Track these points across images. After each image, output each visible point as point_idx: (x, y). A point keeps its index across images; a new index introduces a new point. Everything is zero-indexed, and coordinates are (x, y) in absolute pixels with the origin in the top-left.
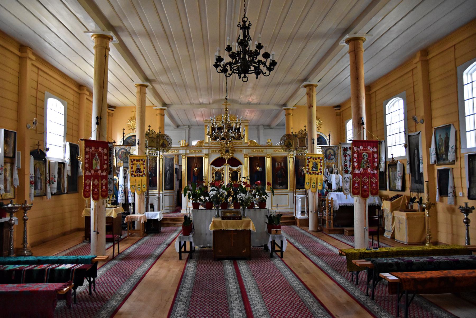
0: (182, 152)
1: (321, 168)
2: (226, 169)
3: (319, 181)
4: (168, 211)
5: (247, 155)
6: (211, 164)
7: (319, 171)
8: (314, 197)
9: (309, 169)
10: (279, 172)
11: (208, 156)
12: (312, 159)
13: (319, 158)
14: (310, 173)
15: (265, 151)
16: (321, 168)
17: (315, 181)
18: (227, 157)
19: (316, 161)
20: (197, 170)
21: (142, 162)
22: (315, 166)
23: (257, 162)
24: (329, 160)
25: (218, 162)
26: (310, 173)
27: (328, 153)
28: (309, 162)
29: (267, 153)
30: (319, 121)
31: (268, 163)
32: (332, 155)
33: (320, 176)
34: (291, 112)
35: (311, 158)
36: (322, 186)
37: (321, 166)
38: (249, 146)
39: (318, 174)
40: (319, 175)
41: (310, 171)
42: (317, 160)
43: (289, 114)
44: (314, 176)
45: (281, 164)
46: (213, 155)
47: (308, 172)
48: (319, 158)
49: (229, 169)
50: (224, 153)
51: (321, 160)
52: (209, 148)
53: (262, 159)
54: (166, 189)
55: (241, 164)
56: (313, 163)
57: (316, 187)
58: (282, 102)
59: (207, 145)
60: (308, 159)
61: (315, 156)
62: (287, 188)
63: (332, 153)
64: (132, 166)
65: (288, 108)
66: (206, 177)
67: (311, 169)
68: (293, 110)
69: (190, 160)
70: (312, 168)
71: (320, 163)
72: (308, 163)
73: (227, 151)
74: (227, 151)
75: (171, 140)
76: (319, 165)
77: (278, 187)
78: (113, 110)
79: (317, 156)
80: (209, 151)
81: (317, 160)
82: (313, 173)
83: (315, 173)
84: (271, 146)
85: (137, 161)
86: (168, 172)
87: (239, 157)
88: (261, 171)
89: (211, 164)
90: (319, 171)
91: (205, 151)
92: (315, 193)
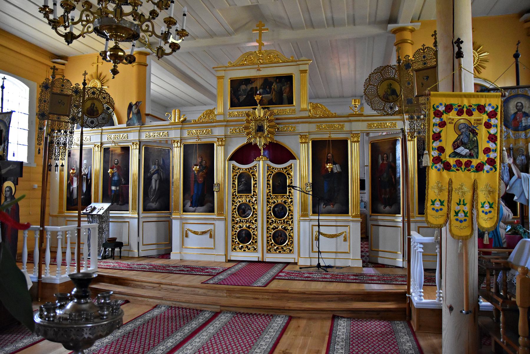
0: (174, 134)
2: (261, 167)
3: (482, 197)
4: (154, 253)
5: (305, 137)
6: (231, 159)
7: (482, 158)
8: (462, 256)
9: (441, 150)
10: (385, 175)
11: (224, 141)
12: (453, 115)
14: (447, 167)
15: (347, 127)
16: (491, 145)
17: (468, 197)
18: (260, 142)
19: (472, 119)
20: (199, 171)
22: (467, 138)
23: (329, 153)
24: (516, 129)
25: (244, 155)
26: (447, 167)
28: (443, 124)
29: (351, 132)
30: (480, 53)
33: (483, 178)
34: (407, 35)
35: (449, 108)
36: (494, 214)
37: (492, 138)
38: (309, 117)
39: (479, 168)
40: (483, 175)
41: (446, 157)
42: (476, 115)
43: (404, 41)
44: (462, 178)
45: (387, 157)
46: (235, 139)
47: (437, 160)
49: (269, 167)
50: (253, 133)
51: (492, 115)
52: (226, 123)
53: (341, 147)
54: (146, 209)
55: (294, 158)
56: (457, 127)
57: (471, 217)
58: (383, 13)
59: (221, 118)
60: (438, 114)
61: (466, 102)
62: (345, 211)
64: (437, 129)
65: (400, 25)
66: (218, 185)
67: (449, 150)
68: (412, 31)
69: (187, 149)
70: (456, 145)
72: (437, 129)
73: (260, 129)
74: (260, 129)
76: (483, 133)
77: (381, 207)
78: (64, 64)
80: (226, 131)
81: (476, 115)
84: (361, 115)
85: (460, 113)
86: (155, 176)
87: (288, 142)
88: (339, 173)
89: (231, 159)
90: (482, 158)
91: (219, 132)
92: (465, 240)
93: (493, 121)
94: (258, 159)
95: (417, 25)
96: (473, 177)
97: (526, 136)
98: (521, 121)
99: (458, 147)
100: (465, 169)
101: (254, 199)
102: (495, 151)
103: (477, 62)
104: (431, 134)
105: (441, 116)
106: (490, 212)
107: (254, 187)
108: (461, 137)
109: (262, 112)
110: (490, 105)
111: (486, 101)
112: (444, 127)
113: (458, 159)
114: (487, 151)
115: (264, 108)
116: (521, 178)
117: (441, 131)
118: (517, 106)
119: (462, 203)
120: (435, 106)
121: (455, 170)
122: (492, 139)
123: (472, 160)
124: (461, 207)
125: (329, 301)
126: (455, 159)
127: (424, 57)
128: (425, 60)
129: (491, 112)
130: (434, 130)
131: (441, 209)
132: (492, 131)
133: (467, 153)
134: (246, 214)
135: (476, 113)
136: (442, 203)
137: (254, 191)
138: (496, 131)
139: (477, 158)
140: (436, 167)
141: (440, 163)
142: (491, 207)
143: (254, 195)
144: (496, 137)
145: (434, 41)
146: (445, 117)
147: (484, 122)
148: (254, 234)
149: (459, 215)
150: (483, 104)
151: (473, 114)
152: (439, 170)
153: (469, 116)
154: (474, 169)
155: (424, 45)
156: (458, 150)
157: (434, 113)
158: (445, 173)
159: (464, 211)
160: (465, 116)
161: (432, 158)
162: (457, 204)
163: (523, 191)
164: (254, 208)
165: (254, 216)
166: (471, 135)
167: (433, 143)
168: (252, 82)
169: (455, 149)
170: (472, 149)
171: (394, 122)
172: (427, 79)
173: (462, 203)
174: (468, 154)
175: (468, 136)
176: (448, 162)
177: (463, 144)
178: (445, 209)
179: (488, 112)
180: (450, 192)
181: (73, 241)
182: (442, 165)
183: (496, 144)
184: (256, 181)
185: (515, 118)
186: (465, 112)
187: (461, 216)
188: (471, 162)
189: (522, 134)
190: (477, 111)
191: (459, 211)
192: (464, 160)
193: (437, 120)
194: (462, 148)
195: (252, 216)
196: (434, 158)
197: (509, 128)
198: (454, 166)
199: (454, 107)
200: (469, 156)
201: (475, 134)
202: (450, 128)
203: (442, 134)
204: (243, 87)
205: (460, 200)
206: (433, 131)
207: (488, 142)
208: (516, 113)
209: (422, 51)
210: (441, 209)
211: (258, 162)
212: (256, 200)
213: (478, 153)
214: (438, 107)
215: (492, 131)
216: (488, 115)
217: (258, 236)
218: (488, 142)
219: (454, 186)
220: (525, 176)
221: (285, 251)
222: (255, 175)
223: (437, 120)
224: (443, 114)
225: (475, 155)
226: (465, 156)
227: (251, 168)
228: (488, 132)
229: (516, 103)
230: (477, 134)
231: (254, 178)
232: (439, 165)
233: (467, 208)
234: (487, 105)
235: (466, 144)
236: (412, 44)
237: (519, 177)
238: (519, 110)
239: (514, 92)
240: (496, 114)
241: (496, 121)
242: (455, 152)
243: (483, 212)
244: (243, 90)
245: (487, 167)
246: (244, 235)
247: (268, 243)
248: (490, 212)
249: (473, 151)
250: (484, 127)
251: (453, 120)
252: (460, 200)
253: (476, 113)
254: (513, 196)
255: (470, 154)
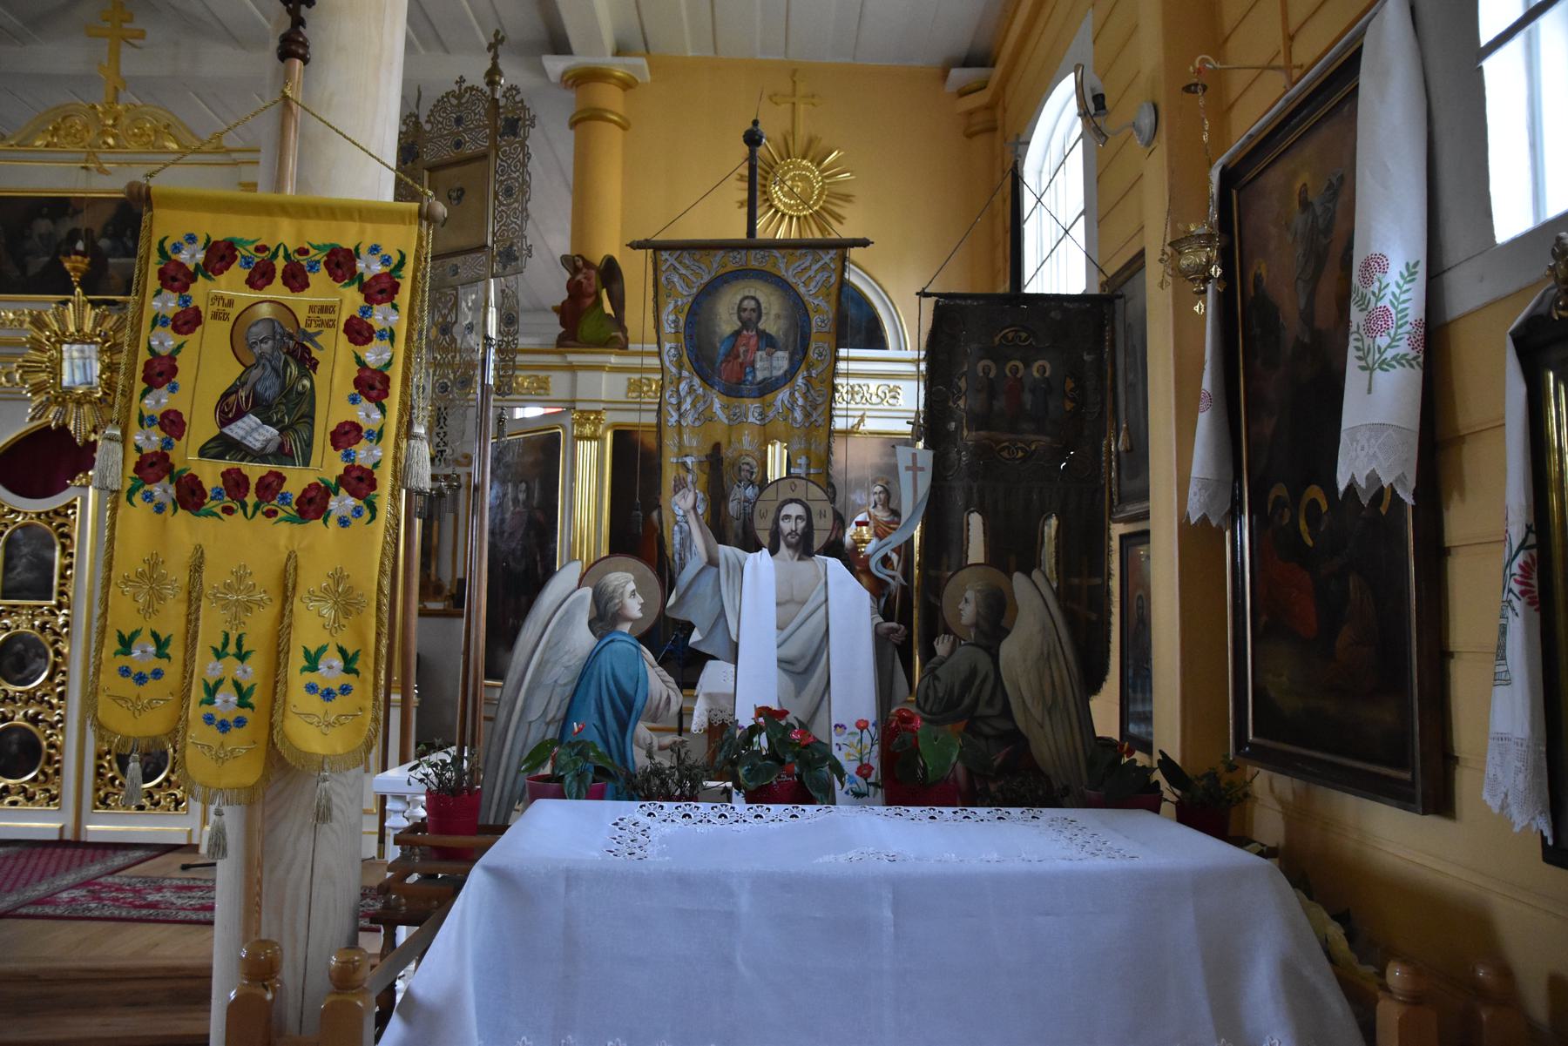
1: (364, 414)
3: (312, 624)
7: (328, 464)
9: (173, 424)
12: (232, 285)
13: (341, 263)
14: (190, 496)
16: (364, 414)
17: (258, 628)
19: (301, 302)
21: (350, 300)
22: (277, 383)
24: (733, 391)
27: (726, 320)
28: (188, 321)
31: (332, 316)
32: (769, 342)
34: (610, 98)
35: (221, 255)
37: (371, 385)
39: (312, 505)
41: (186, 455)
48: (341, 263)
51: (381, 290)
56: (239, 341)
61: (286, 234)
63: (771, 324)
64: (167, 341)
67: (203, 427)
68: (627, 85)
70: (228, 411)
71: (358, 332)
72: (167, 341)
75: (1016, 610)
76: (337, 365)
79: (320, 234)
81: (321, 289)
82: (235, 484)
83: (270, 487)
85: (260, 276)
93: (380, 317)
94: (80, 479)
95: (636, 65)
96: (283, 542)
97: (763, 415)
98: (752, 364)
99: (240, 414)
100: (257, 507)
101: (61, 620)
102: (379, 436)
103: (820, 195)
104: (143, 356)
105: (186, 288)
106: (345, 690)
107: (63, 576)
108: (256, 373)
109: (90, 315)
110: (374, 249)
111: (362, 232)
112: (191, 331)
113: (235, 464)
114: (346, 435)
115: (95, 304)
116: (717, 566)
117: (179, 348)
118: (741, 309)
119: (232, 648)
120: (168, 245)
121: (218, 510)
122: (372, 387)
123: (287, 470)
124: (231, 669)
125: (133, 1005)
126: (224, 465)
127: (459, 121)
128: (458, 133)
129: (377, 277)
130: (155, 343)
131: (157, 674)
132: (373, 355)
133: (268, 441)
134: (27, 672)
135: (319, 279)
136: (161, 645)
137: (62, 593)
138: (386, 356)
139: (306, 463)
140: (148, 497)
141: (166, 480)
142: (349, 669)
143: (60, 606)
144: (386, 381)
145: (489, 65)
146: (200, 291)
147: (344, 317)
148: (51, 746)
149: (219, 700)
150: (349, 244)
151: (308, 285)
152: (160, 509)
153: (293, 290)
154: (292, 509)
155: (462, 80)
156: (236, 430)
157: (162, 274)
158: (181, 521)
159: (237, 685)
160: (277, 290)
161: (134, 457)
162: (215, 650)
163: (722, 614)
164: (58, 653)
165: (58, 679)
166: (293, 370)
167: (143, 395)
168: (77, 212)
169: (225, 421)
170: (291, 426)
171: (542, 374)
172: (459, 198)
173: (232, 648)
174: (271, 448)
175: (280, 373)
176: (194, 478)
177: (262, 408)
178: (173, 670)
179: (366, 278)
180: (193, 599)
181: (490, 724)
182: (172, 491)
183: (383, 410)
184: (71, 555)
185: (732, 354)
186: (279, 274)
187: (226, 701)
188: (281, 478)
189: (752, 408)
190: (324, 272)
191: (219, 682)
192: (255, 471)
193: (170, 304)
194: (251, 420)
195: (50, 678)
196: (143, 457)
197: (712, 387)
198: (218, 494)
199: (241, 252)
200: (273, 454)
201: (308, 364)
202: (215, 333)
203: (182, 361)
204: (43, 226)
205: (227, 636)
206: (150, 349)
207: (354, 400)
208: (737, 334)
209: (454, 102)
210: (157, 674)
211: (82, 490)
212: (66, 624)
213: (309, 444)
214: (177, 248)
215: (373, 355)
216: (363, 288)
217: (67, 754)
218: (354, 400)
219: (212, 578)
220: (732, 559)
221: (157, 804)
222: (68, 536)
223: (170, 304)
224: (194, 280)
225: (297, 451)
226: (260, 456)
227: (56, 512)
228: (359, 360)
229: (739, 298)
230: (314, 365)
231: (64, 547)
232: (163, 490)
233: (252, 672)
234: (363, 251)
235: (269, 407)
236: (624, 128)
237: (712, 562)
238: (745, 324)
239: (732, 262)
240: (395, 288)
241: (393, 318)
242: (222, 433)
243: (311, 688)
244: (41, 236)
245: (342, 503)
246: (14, 748)
247: (99, 775)
248: (345, 690)
249: (291, 437)
250: (343, 338)
251: (231, 303)
252: (227, 636)
253: (319, 279)
254: (689, 627)
255: (281, 446)
